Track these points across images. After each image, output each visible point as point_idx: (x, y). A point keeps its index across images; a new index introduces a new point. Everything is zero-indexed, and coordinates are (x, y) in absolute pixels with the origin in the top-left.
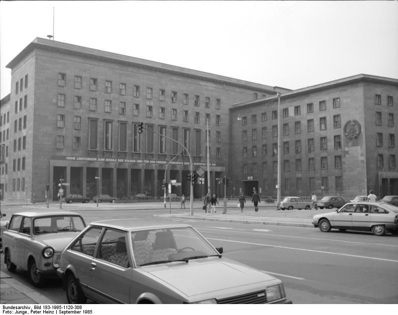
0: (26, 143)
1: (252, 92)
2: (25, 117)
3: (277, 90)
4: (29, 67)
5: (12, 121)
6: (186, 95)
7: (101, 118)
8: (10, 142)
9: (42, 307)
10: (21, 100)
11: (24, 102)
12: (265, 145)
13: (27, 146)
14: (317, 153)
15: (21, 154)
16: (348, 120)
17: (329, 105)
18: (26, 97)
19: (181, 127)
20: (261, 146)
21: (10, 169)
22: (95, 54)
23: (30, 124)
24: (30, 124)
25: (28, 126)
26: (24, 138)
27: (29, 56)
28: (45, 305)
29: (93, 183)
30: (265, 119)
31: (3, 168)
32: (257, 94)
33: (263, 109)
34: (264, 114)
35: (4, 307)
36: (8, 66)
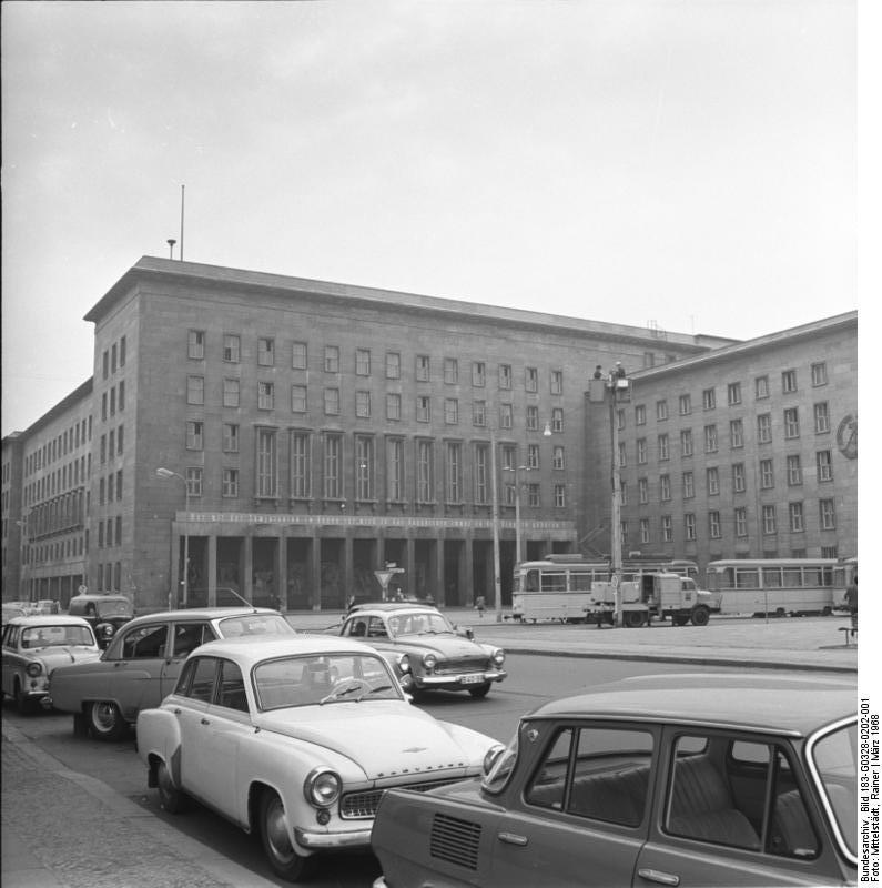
0: (123, 488)
1: (640, 352)
2: (121, 428)
3: (702, 344)
4: (128, 319)
5: (96, 437)
6: (480, 366)
7: (283, 425)
8: (93, 483)
9: (866, 794)
10: (113, 390)
11: (116, 399)
12: (666, 477)
13: (124, 492)
14: (782, 497)
15: (113, 510)
16: (847, 414)
17: (804, 380)
18: (122, 384)
19: (468, 440)
20: (658, 479)
21: (94, 544)
22: (269, 285)
23: (130, 442)
24: (130, 442)
25: (126, 448)
26: (120, 473)
27: (129, 297)
28: (859, 788)
29: (269, 573)
30: (793, 389)
31: (81, 539)
32: (652, 355)
33: (684, 386)
34: (661, 403)
35: (865, 879)
36: (88, 318)
